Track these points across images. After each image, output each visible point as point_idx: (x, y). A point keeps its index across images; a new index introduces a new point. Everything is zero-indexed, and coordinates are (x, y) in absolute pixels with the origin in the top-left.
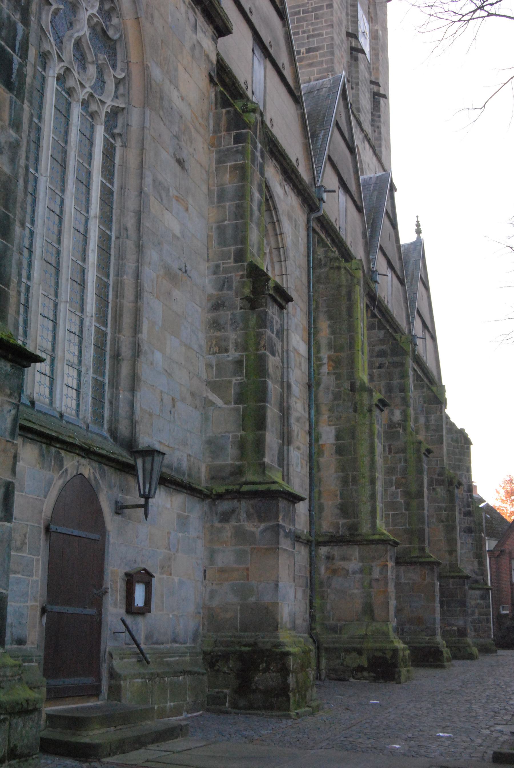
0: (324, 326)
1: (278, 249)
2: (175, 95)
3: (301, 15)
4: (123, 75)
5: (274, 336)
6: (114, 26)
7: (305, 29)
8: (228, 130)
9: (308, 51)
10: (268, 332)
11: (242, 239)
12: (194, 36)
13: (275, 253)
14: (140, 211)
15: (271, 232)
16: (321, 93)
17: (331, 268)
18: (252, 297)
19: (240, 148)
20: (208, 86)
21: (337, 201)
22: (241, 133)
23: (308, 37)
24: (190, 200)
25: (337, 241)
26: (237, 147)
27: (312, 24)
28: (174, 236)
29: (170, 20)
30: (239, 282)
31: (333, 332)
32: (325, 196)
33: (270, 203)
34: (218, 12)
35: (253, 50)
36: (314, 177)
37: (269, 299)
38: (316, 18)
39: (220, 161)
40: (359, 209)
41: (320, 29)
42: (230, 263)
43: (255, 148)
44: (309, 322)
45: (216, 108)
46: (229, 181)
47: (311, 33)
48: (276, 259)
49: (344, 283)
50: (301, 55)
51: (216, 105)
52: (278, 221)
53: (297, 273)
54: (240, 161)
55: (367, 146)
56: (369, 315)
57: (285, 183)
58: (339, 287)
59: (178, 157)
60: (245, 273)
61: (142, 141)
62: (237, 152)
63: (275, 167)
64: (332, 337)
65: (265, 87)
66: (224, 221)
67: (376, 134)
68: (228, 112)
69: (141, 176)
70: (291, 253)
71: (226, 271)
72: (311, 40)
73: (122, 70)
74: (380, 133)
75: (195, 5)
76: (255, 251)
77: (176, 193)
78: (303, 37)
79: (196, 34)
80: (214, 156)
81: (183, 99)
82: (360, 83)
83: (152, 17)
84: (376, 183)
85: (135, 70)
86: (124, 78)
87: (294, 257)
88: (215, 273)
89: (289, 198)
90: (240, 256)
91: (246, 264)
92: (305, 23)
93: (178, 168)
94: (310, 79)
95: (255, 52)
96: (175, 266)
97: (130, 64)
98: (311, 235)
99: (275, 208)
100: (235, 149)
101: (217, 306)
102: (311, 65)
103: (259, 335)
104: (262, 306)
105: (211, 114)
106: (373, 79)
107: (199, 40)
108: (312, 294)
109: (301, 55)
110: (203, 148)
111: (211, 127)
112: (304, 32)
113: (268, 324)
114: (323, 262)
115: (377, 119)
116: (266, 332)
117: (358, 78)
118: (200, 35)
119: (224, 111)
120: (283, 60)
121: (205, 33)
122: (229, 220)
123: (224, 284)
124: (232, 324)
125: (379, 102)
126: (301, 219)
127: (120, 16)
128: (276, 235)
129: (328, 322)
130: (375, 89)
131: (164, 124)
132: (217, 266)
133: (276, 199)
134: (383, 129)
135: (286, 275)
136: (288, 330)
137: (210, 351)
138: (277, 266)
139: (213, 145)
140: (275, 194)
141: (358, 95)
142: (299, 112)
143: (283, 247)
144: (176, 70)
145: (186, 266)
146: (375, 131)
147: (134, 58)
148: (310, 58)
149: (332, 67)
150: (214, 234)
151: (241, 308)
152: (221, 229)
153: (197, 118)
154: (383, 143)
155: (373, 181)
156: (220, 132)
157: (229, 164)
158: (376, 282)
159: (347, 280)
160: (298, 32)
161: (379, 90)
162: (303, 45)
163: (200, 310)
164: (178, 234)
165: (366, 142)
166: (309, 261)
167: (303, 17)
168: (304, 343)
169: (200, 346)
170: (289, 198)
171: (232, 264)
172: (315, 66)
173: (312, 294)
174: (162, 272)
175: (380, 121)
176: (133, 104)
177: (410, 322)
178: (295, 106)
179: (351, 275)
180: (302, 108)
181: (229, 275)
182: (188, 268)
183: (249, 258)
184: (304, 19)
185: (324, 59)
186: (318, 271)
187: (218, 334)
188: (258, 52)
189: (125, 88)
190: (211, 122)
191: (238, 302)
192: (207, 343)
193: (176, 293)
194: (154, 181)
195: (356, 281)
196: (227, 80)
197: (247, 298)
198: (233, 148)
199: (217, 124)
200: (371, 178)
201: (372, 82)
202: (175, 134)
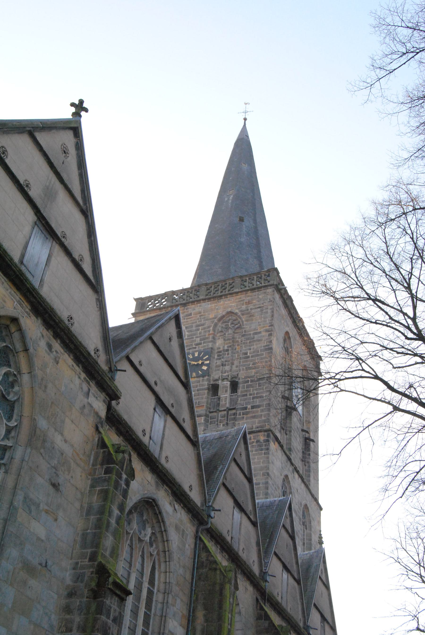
0: (200, 614)
1: (164, 552)
2: (58, 440)
3: (250, 383)
4: (16, 424)
5: (110, 621)
6: (14, 392)
7: (251, 392)
8: (102, 464)
9: (253, 407)
10: (103, 618)
11: (96, 543)
12: (86, 400)
13: (162, 555)
14: (7, 519)
15: (159, 539)
16: (227, 439)
17: (210, 569)
18: (96, 589)
19: (107, 477)
20: (94, 434)
21: (231, 517)
22: (110, 467)
23: (253, 398)
24: (61, 514)
25: (225, 547)
26: (106, 477)
27: (256, 390)
28: (39, 539)
29: (63, 388)
30: (88, 577)
31: (206, 621)
32: (212, 514)
33: (159, 517)
34: (108, 384)
35: (155, 409)
36: (205, 499)
37: (108, 592)
38: (260, 386)
39: (92, 486)
40: (254, 524)
41: (262, 393)
42: (86, 562)
43: (121, 478)
44: (190, 611)
45: (97, 449)
46: (96, 501)
47: (255, 395)
48: (162, 559)
49: (218, 581)
50: (248, 410)
51: (97, 447)
52: (165, 531)
53: (181, 571)
54: (106, 486)
55: (296, 476)
56: (258, 608)
57: (175, 503)
58: (215, 584)
59: (53, 482)
60: (95, 570)
61: (20, 469)
62: (105, 480)
63: (166, 490)
64: (205, 624)
65: (163, 434)
66: (87, 530)
67: (307, 467)
68: (104, 452)
69: (14, 494)
70: (175, 556)
71: (82, 567)
72: (255, 400)
73: (16, 421)
74: (309, 467)
75: (90, 379)
76: (107, 554)
77: (46, 508)
78: (250, 398)
79: (88, 399)
80: (89, 482)
81: (66, 441)
82: (292, 431)
83: (46, 387)
84: (278, 505)
85: (26, 423)
86: (16, 425)
87: (179, 558)
88: (74, 569)
89: (179, 514)
90: (93, 557)
91: (96, 563)
92: (252, 389)
93: (52, 490)
94: (252, 426)
95: (157, 410)
96: (35, 562)
97: (22, 417)
98: (198, 542)
99: (163, 521)
100: (104, 478)
101: (71, 594)
102: (254, 417)
103: (95, 620)
104: (101, 597)
105: (93, 453)
106: (305, 428)
107: (90, 402)
108: (194, 589)
109: (248, 410)
110: (81, 476)
111: (91, 462)
112: (250, 395)
113: (104, 611)
114: (205, 564)
115: (307, 456)
116: (101, 617)
117: (291, 427)
118: (91, 399)
119: (102, 451)
120: (184, 415)
121: (97, 398)
122: (91, 530)
123: (78, 578)
124: (78, 610)
125: (310, 444)
126: (190, 530)
127: (21, 385)
128: (164, 541)
129: (204, 612)
130: (307, 435)
131: (43, 459)
132: (77, 563)
133: (164, 514)
134: (312, 465)
135: (170, 572)
136: (165, 616)
137: (59, 630)
138: (163, 565)
139: (90, 474)
140: (163, 511)
141: (290, 439)
142: (196, 452)
143: (168, 551)
144: (63, 422)
145: (46, 562)
146: (305, 465)
147: (26, 412)
148: (254, 412)
149: (268, 419)
150: (79, 539)
151: (87, 598)
152: (84, 536)
153: (78, 455)
154: (312, 475)
155: (277, 503)
156: (96, 465)
157: (98, 489)
158: (266, 581)
159: (220, 580)
160: (247, 394)
161: (310, 436)
162: (249, 403)
163: (56, 596)
164: (43, 538)
165: (295, 473)
166: (194, 562)
167: (251, 385)
168: (181, 628)
169: (52, 626)
170: (179, 514)
171: (87, 563)
172: (257, 418)
173: (194, 589)
174: (20, 565)
175: (309, 458)
176: (20, 444)
177: (306, 615)
178: (193, 448)
179: (224, 575)
180: (198, 449)
181: (84, 571)
182: (50, 563)
183: (100, 559)
184: (251, 386)
185: (263, 413)
186: (201, 571)
187: (68, 617)
188: (159, 410)
189: (15, 432)
190: (92, 458)
191: (86, 591)
192: (59, 623)
193: (32, 582)
194: (25, 498)
195: (227, 580)
196: (122, 429)
197: (92, 590)
198: (102, 477)
199: (96, 459)
200: (275, 501)
201: (303, 430)
202: (53, 465)
